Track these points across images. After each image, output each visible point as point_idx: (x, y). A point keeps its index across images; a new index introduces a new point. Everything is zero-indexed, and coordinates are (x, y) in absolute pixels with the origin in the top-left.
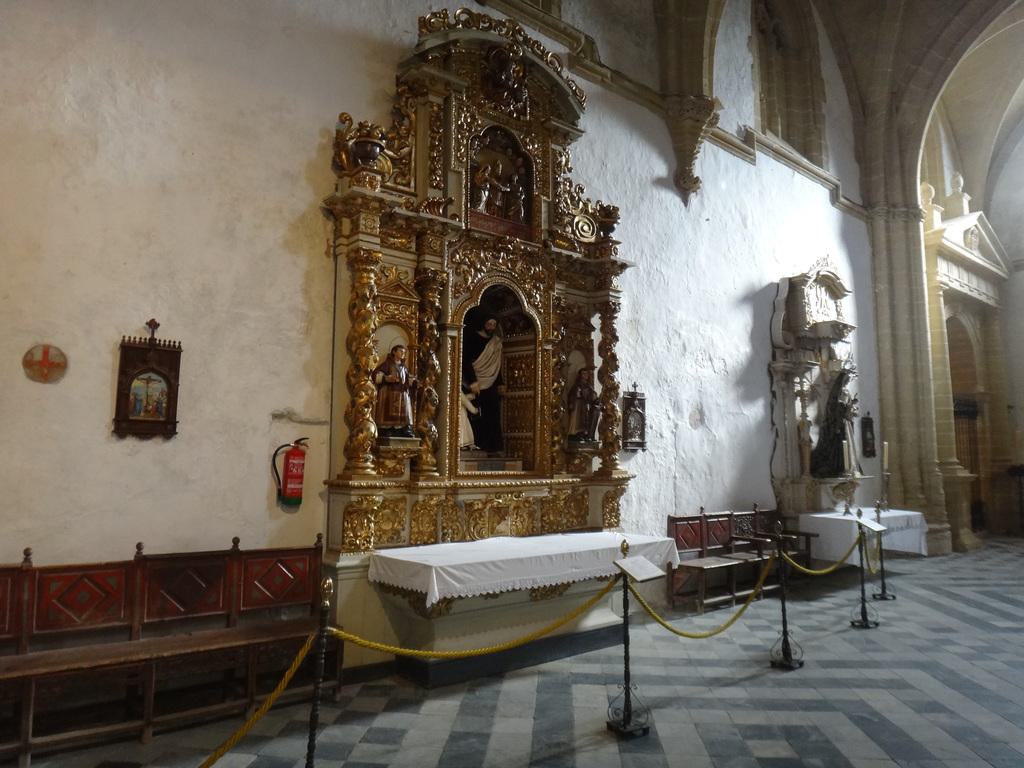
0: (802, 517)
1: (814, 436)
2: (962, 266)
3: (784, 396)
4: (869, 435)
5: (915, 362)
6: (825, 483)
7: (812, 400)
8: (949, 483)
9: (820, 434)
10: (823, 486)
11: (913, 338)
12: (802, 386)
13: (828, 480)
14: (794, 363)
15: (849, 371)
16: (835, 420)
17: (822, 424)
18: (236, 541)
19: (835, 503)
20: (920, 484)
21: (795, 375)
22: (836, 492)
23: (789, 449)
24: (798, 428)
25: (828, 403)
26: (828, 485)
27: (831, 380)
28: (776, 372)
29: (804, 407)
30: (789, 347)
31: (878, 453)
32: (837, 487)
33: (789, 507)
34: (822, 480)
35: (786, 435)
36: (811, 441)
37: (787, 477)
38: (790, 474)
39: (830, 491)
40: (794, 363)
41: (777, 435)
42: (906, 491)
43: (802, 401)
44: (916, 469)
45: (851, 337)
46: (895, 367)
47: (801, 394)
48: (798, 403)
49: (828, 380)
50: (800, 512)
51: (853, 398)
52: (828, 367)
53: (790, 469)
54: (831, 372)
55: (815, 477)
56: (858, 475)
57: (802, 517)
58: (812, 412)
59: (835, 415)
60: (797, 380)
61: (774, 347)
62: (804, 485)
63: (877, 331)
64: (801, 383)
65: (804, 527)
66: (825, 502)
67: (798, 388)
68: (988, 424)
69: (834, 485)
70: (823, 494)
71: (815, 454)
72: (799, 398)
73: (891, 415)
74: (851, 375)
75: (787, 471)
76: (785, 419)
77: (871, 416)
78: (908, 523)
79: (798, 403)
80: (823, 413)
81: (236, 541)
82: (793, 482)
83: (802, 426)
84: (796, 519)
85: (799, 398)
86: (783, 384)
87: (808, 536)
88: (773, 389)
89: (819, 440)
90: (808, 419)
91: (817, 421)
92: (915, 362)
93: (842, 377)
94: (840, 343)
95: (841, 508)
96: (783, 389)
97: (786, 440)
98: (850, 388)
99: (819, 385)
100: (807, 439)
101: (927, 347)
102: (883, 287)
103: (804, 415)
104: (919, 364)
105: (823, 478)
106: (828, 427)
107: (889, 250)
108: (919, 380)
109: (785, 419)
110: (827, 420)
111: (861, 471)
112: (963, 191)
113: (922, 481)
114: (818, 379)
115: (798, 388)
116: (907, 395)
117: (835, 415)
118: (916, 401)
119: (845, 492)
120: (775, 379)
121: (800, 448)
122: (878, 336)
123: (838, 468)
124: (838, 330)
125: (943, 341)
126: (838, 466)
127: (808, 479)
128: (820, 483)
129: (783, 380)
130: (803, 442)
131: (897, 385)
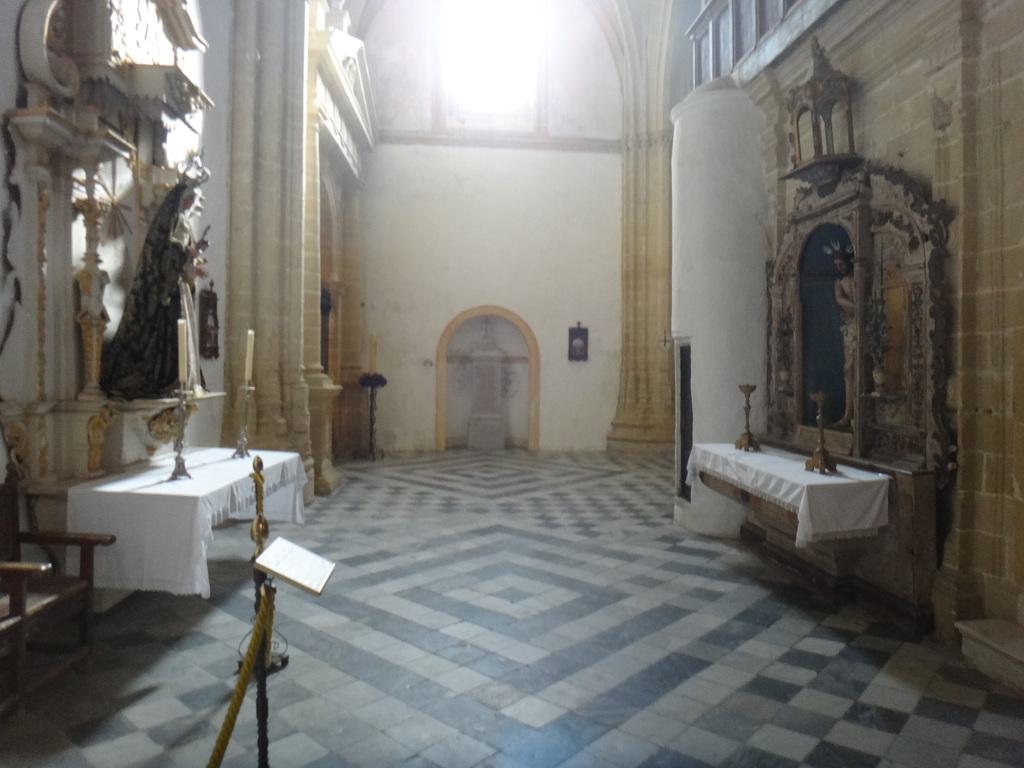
0: (75, 492)
1: (113, 306)
2: (338, 107)
3: (43, 204)
4: (210, 322)
5: (283, 215)
6: (134, 410)
7: (113, 233)
8: (315, 397)
9: (126, 307)
10: (127, 416)
11: (283, 173)
12: (90, 191)
13: (138, 403)
14: (76, 131)
15: (196, 183)
16: (162, 277)
17: (131, 284)
18: (579, 323)
19: (151, 450)
20: (280, 402)
21: (77, 163)
22: (157, 426)
23: (49, 331)
24: (76, 285)
25: (148, 241)
26: (139, 415)
27: (153, 204)
28: (26, 141)
29: (92, 240)
30: (66, 92)
31: (222, 351)
32: (155, 418)
33: (43, 472)
34: (127, 404)
35: (42, 298)
36: (104, 317)
37: (42, 398)
38: (49, 390)
39: (143, 426)
40: (76, 131)
41: (18, 297)
42: (259, 414)
43: (90, 224)
44: (275, 380)
45: (197, 118)
46: (255, 217)
47: (88, 208)
48: (79, 230)
49: (147, 202)
50: (72, 478)
51: (197, 238)
52: (148, 177)
53: (48, 379)
54: (155, 188)
55: (110, 396)
56: (199, 392)
57: (75, 492)
58: (110, 259)
59: (160, 268)
60: (80, 175)
61: (23, 76)
62: (86, 417)
63: (231, 177)
64: (89, 185)
65: (80, 518)
66: (131, 451)
67: (79, 194)
68: (340, 323)
69: (152, 414)
70: (127, 431)
71: (110, 349)
72: (81, 218)
73: (244, 292)
74: (198, 191)
75: (42, 383)
76: (41, 259)
77: (215, 289)
78: (282, 476)
79: (79, 230)
80: (135, 261)
81: (579, 323)
82: (54, 410)
83: (88, 281)
84: (61, 498)
85: (81, 218)
86: (44, 173)
87: (88, 546)
88: (13, 180)
89: (124, 320)
90: (101, 267)
91: (122, 280)
92: (283, 215)
93: (179, 195)
94: (179, 121)
95: (165, 459)
96: (41, 186)
97: (42, 308)
98: (190, 220)
99: (128, 208)
100: (98, 313)
101: (301, 195)
102: (250, 56)
103: (92, 258)
104: (288, 218)
105: (130, 399)
106: (146, 291)
107: (260, 28)
108: (287, 243)
109: (41, 259)
110: (143, 276)
111: (203, 384)
112: (344, 7)
113: (283, 398)
114: (127, 195)
115: (79, 194)
116: (269, 266)
117: (160, 268)
118: (281, 274)
119: (170, 427)
120: (21, 156)
121: (78, 329)
122: (232, 159)
123: (165, 379)
124: (178, 94)
125: (315, 195)
126: (162, 376)
127: (93, 400)
128: (122, 410)
129: (40, 163)
130: (85, 320)
131: (256, 246)
